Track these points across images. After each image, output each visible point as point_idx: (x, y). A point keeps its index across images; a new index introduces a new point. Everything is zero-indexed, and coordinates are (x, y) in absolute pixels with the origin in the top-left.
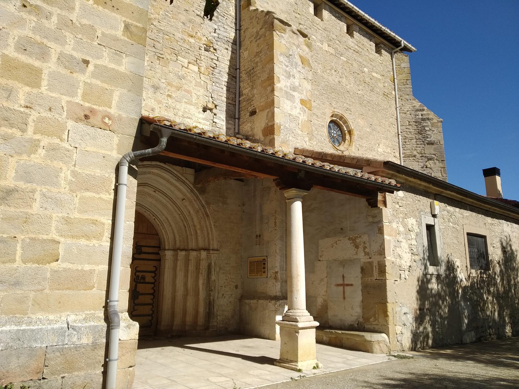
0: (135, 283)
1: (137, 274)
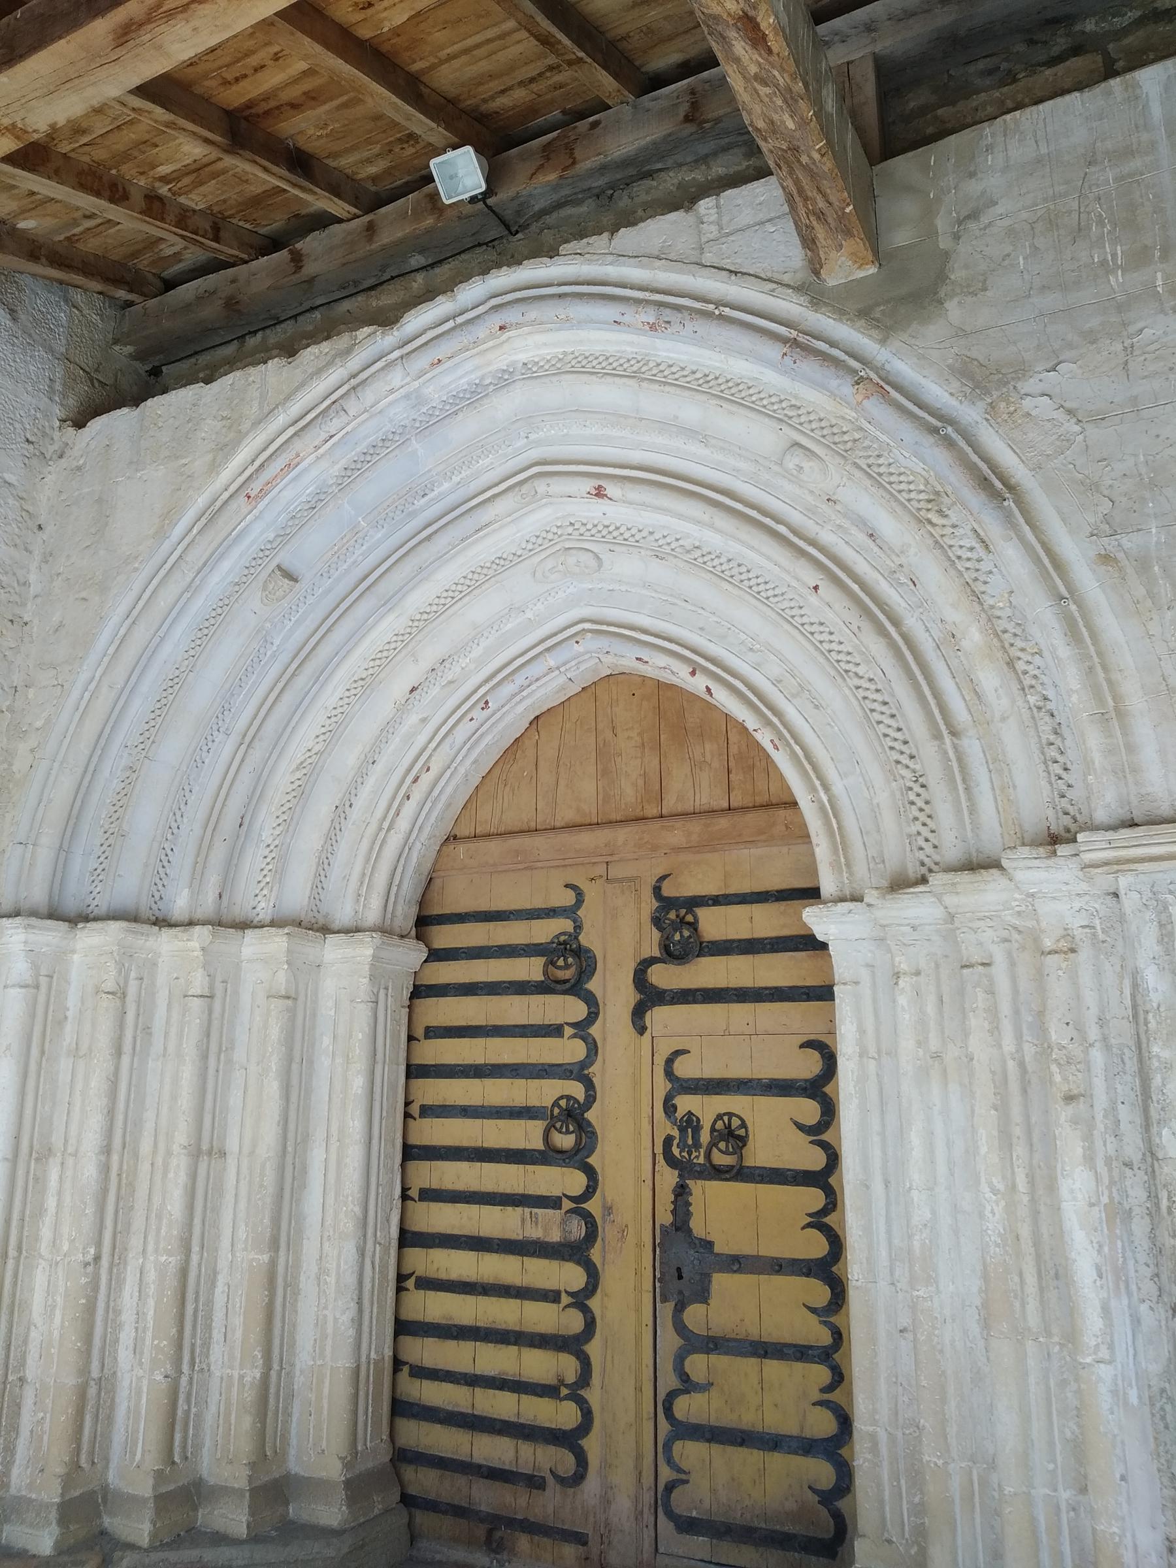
0: (669, 1178)
1: (686, 1103)
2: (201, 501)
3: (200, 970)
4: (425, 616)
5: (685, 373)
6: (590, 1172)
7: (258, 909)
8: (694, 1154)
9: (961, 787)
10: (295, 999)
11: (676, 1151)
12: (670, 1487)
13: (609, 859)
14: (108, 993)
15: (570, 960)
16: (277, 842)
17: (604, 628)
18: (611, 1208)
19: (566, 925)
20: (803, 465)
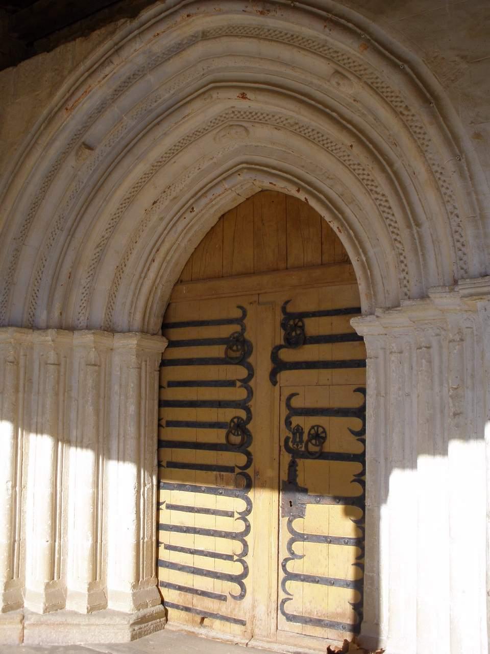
0: (287, 458)
1: (296, 421)
2: (45, 112)
3: (53, 351)
4: (159, 164)
5: (281, 35)
6: (248, 454)
7: (81, 320)
8: (300, 446)
9: (420, 253)
10: (99, 366)
11: (291, 444)
12: (284, 602)
13: (259, 292)
14: (11, 362)
15: (239, 347)
16: (88, 286)
17: (253, 166)
18: (258, 472)
19: (237, 328)
20: (340, 82)
